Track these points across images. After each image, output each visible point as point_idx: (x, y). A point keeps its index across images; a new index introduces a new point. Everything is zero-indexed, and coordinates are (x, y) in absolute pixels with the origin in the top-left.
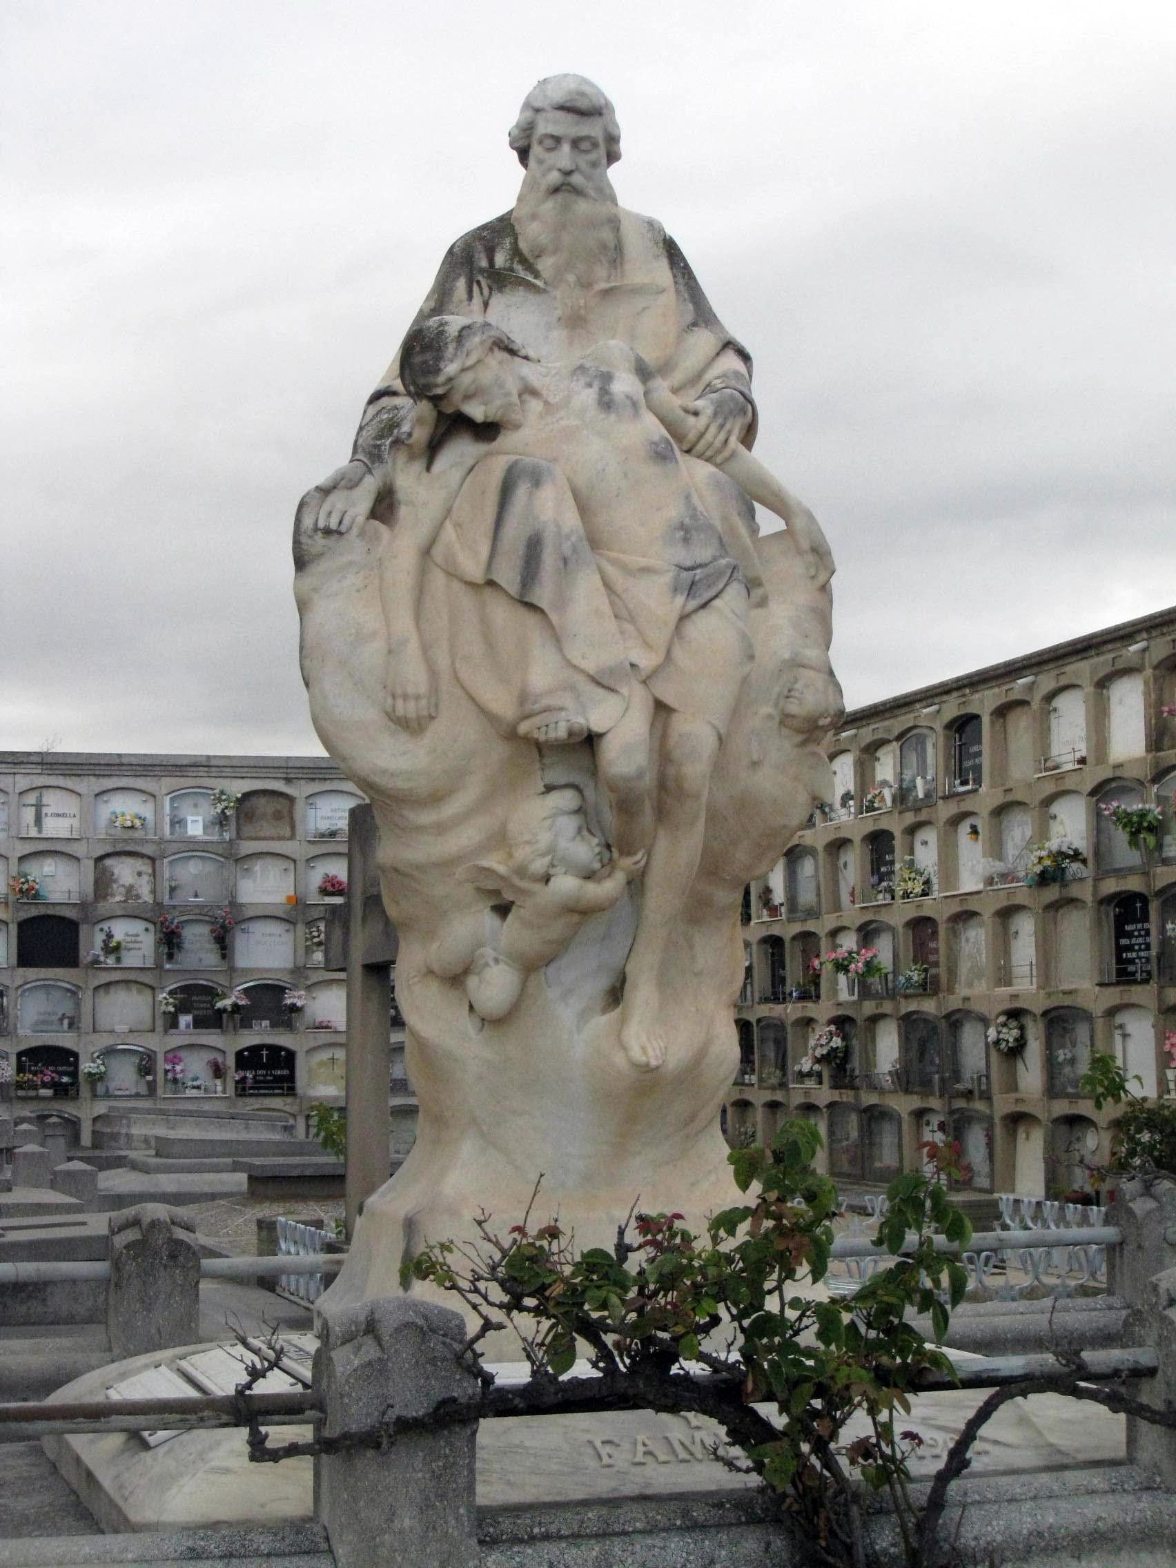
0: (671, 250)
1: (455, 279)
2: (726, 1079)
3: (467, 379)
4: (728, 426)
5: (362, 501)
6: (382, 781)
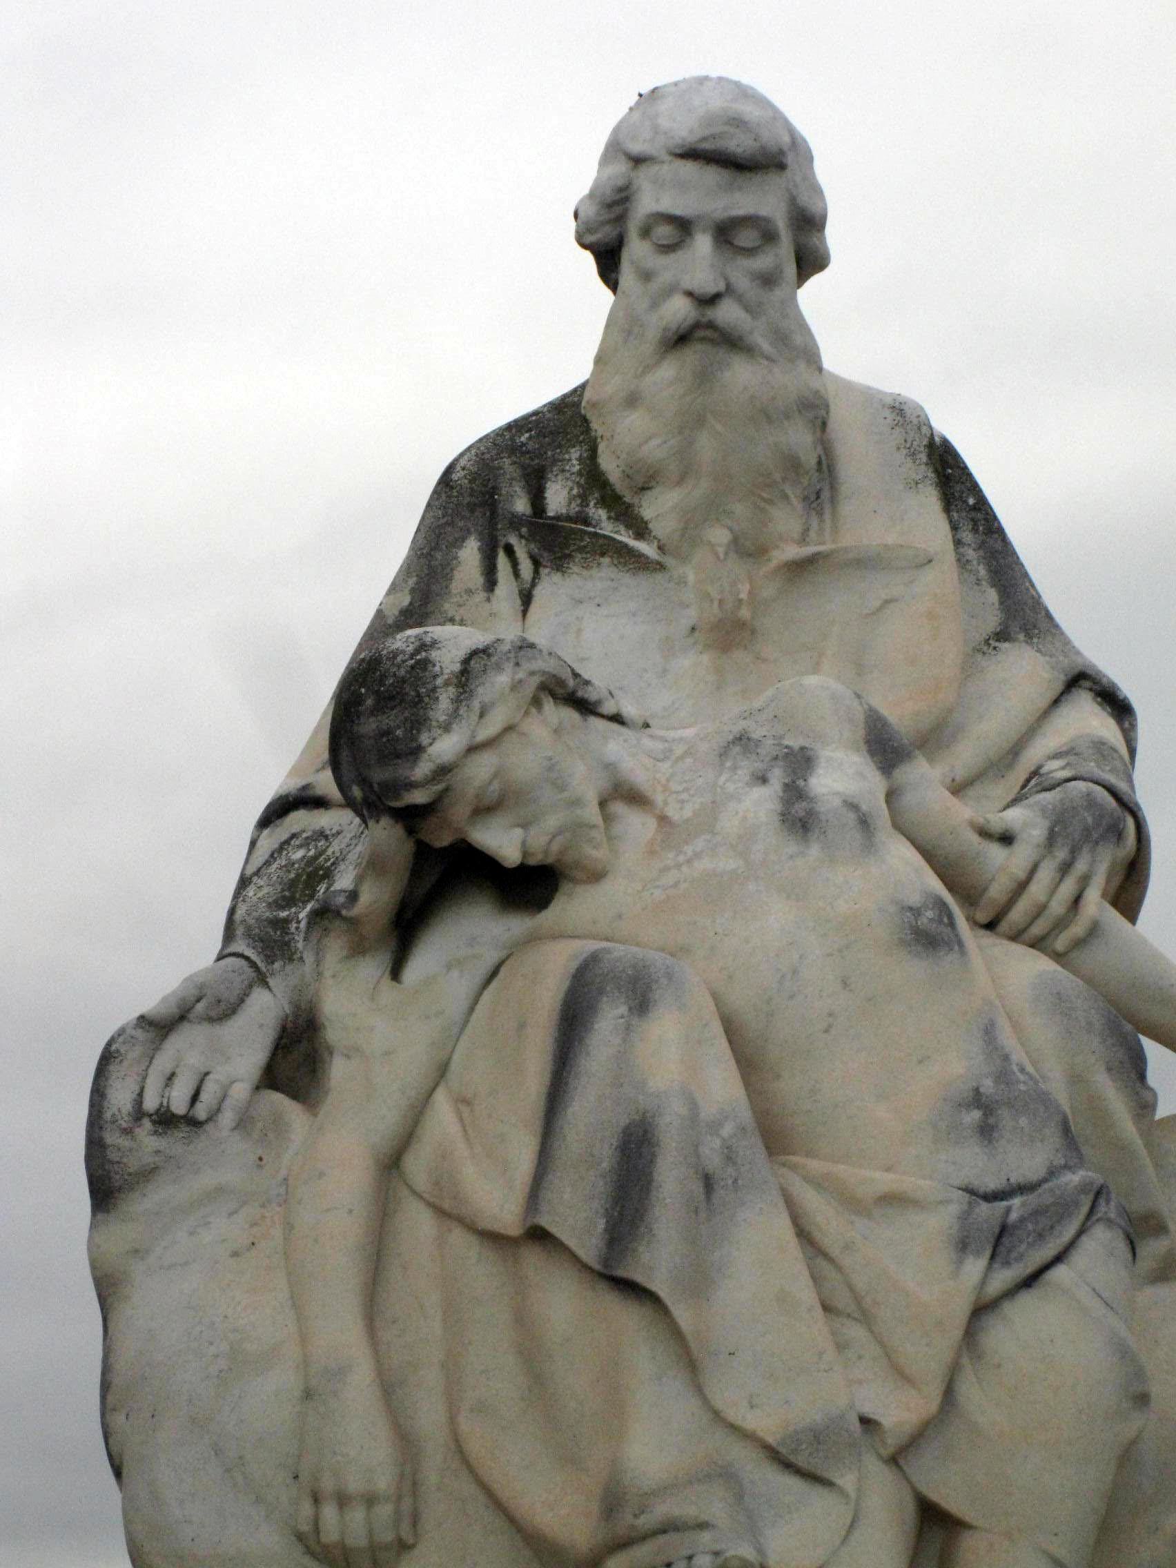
0: (947, 470)
3: (481, 770)
4: (1081, 866)
5: (244, 1045)
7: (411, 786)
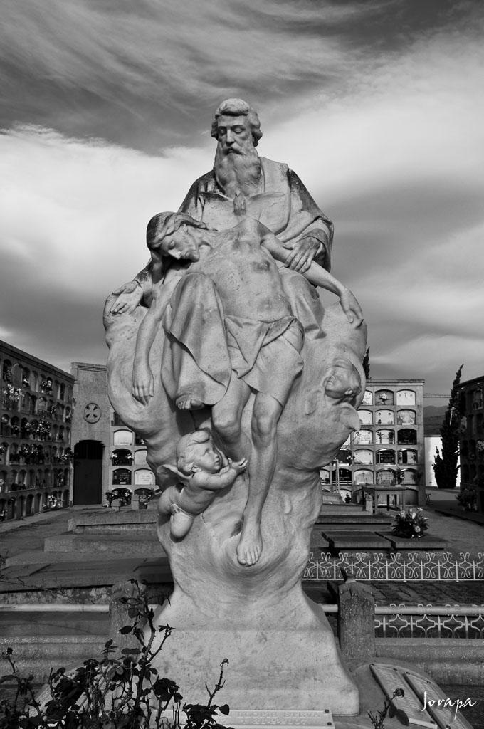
0: (292, 177)
1: (191, 198)
2: (301, 565)
3: (168, 239)
4: (306, 254)
5: (135, 298)
6: (139, 427)
7: (154, 244)
